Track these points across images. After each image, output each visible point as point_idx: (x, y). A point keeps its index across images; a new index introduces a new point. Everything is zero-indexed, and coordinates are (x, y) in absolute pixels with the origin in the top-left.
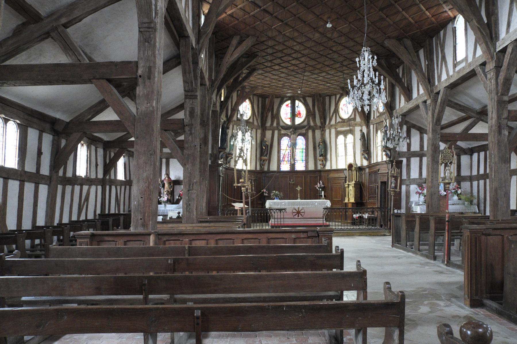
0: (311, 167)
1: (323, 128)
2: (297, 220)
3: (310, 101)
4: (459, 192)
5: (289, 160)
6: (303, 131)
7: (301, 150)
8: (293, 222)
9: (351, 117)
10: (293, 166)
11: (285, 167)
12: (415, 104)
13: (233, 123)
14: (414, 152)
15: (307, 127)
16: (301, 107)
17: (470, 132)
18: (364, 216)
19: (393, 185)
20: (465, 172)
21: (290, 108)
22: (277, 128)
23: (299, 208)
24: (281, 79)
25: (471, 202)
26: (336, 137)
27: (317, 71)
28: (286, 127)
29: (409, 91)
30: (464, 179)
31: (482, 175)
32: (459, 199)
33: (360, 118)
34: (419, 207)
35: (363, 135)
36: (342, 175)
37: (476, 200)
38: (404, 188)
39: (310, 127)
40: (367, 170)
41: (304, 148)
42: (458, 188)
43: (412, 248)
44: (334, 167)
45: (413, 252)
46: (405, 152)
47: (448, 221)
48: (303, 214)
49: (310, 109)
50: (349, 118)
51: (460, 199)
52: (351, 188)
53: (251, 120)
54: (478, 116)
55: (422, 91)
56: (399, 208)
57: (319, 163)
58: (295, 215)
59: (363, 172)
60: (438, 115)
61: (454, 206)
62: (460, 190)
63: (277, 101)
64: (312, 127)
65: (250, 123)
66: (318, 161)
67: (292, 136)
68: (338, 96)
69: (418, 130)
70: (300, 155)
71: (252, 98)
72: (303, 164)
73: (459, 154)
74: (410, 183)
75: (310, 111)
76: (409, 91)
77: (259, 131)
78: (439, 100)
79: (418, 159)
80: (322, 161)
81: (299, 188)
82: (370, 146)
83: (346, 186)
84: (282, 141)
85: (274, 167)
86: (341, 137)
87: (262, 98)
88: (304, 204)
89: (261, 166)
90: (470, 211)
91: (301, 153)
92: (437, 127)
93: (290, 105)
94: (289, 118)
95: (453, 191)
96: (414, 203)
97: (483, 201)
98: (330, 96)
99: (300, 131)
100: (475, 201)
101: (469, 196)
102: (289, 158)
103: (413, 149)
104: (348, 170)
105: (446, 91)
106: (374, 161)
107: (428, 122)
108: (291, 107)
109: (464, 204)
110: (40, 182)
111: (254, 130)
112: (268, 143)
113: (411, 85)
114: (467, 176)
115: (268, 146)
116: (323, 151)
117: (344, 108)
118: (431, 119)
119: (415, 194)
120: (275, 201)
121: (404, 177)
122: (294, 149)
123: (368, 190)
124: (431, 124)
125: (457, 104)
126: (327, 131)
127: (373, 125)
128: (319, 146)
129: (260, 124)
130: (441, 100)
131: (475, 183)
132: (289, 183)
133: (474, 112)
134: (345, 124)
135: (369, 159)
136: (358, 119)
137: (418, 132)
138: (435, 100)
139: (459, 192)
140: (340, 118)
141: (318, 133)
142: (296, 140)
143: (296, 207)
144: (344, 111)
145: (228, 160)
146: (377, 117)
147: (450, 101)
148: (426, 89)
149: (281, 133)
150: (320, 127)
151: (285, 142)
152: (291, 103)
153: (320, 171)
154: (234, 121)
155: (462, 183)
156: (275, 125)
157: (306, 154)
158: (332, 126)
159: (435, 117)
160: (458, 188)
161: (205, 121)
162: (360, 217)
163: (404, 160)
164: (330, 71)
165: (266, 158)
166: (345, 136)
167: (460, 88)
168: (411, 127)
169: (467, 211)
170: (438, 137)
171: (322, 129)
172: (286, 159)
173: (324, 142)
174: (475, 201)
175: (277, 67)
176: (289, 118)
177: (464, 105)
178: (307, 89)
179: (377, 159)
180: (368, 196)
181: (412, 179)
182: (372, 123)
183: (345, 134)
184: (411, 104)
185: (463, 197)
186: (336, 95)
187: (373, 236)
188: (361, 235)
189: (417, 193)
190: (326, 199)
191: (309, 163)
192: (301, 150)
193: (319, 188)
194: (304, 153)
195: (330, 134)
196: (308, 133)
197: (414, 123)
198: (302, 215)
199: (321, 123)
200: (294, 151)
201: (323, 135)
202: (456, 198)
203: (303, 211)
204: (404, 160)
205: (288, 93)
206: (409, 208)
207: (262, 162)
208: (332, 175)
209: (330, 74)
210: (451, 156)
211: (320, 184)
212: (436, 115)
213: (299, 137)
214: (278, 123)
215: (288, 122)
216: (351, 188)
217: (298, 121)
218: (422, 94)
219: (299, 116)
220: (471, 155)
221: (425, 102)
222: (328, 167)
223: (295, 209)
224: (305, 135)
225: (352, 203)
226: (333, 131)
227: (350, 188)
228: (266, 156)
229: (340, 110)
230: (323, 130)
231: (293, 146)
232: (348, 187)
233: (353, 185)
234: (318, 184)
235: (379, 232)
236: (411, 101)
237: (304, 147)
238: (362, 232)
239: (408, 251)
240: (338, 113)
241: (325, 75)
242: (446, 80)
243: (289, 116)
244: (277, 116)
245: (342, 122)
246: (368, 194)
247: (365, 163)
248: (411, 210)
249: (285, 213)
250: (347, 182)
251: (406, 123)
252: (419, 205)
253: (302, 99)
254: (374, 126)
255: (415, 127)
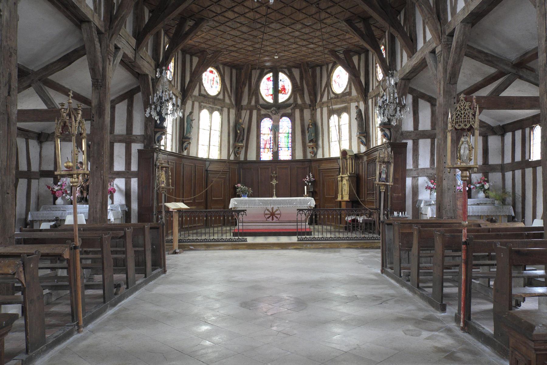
0: (299, 156)
1: (313, 106)
2: (271, 224)
3: (296, 73)
4: (487, 186)
5: (272, 147)
6: (289, 111)
7: (286, 135)
8: (261, 227)
9: (346, 91)
10: (276, 154)
11: (266, 156)
12: (420, 57)
13: (193, 98)
14: (423, 131)
15: (292, 106)
16: (285, 81)
17: (504, 94)
18: (359, 219)
19: (384, 176)
20: (494, 160)
21: (272, 82)
22: (256, 107)
23: (273, 208)
24: (246, 36)
25: (503, 202)
26: (329, 118)
27: (287, 21)
28: (267, 106)
29: (412, 40)
30: (493, 168)
31: (518, 162)
32: (486, 197)
33: (357, 90)
34: (429, 208)
35: (359, 113)
36: (335, 166)
37: (511, 198)
38: (409, 181)
39: (296, 106)
40: (365, 158)
41: (290, 132)
42: (484, 181)
43: (409, 281)
44: (327, 156)
45: (409, 289)
46: (410, 132)
47: (465, 243)
48: (278, 216)
49: (297, 83)
50: (343, 93)
51: (487, 197)
52: (345, 182)
53: (221, 97)
54: (514, 71)
55: (429, 36)
56: (403, 209)
57: (309, 150)
58: (268, 218)
59: (360, 161)
60: (453, 67)
61: (479, 207)
62: (487, 184)
63: (255, 74)
64: (299, 105)
65: (219, 100)
66: (308, 147)
67: (274, 117)
68: (330, 66)
69: (429, 101)
70: (284, 141)
71: (221, 69)
72: (289, 152)
73: (486, 134)
74: (418, 174)
75: (297, 85)
76: (412, 40)
77: (233, 112)
78: (454, 44)
79: (429, 141)
80: (313, 148)
81: (274, 182)
82: (369, 127)
83: (339, 179)
84: (262, 124)
85: (252, 157)
86: (334, 118)
87: (237, 69)
88: (280, 202)
89: (235, 155)
90: (502, 214)
91: (286, 139)
92: (452, 86)
93: (271, 79)
94: (272, 95)
95: (478, 185)
96: (423, 202)
97: (520, 199)
98: (321, 66)
99: (282, 111)
100: (509, 200)
101: (500, 192)
102: (272, 145)
103: (421, 128)
104: (342, 159)
105: (465, 28)
106: (373, 145)
107: (438, 80)
108: (273, 81)
109: (494, 204)
110: (32, 178)
111: (225, 110)
112: (245, 126)
113: (416, 32)
114: (497, 165)
115: (244, 129)
116: (313, 135)
117: (337, 80)
118: (442, 75)
119: (425, 190)
120: (242, 198)
121: (410, 165)
122: (277, 133)
123: (366, 184)
124: (442, 83)
125: (480, 52)
126: (319, 110)
127: (372, 98)
128: (308, 130)
129: (234, 102)
130: (457, 42)
131: (509, 175)
132: (271, 176)
133: (507, 65)
134: (339, 100)
135: (367, 143)
136: (354, 93)
137: (428, 104)
138: (448, 46)
139: (487, 186)
140: (333, 93)
141: (307, 113)
142: (279, 121)
143: (269, 207)
144: (337, 84)
145: (184, 146)
146: (376, 87)
147: (470, 47)
148: (434, 31)
149: (260, 113)
150: (310, 106)
151: (266, 124)
152: (273, 76)
153: (310, 161)
154: (195, 96)
155: (490, 175)
156: (253, 103)
157: (292, 140)
158: (323, 103)
159: (448, 71)
160: (484, 181)
161: (100, 81)
162: (353, 220)
163: (410, 143)
164: (306, 20)
165: (242, 144)
166: (339, 116)
167: (486, 22)
168: (418, 97)
169: (498, 214)
170: (453, 102)
171: (312, 108)
172: (268, 146)
173: (315, 125)
174: (509, 200)
175: (230, 15)
176: (272, 95)
177: (492, 54)
178: (287, 53)
179: (376, 143)
180: (366, 192)
181: (421, 169)
182: (370, 96)
183: (339, 113)
184: (415, 58)
185: (491, 194)
186: (327, 64)
187: (367, 248)
188: (350, 246)
189: (428, 188)
190: (309, 196)
191: (297, 151)
192: (286, 135)
193: (307, 182)
194: (290, 138)
195: (321, 113)
196: (294, 113)
197: (422, 91)
198: (277, 218)
199: (311, 101)
200: (277, 135)
201: (313, 116)
202: (482, 195)
203: (278, 212)
204: (410, 143)
205: (265, 61)
206: (417, 211)
207: (236, 149)
208: (324, 166)
209: (308, 26)
210: (471, 116)
211: (309, 177)
212: (449, 68)
213: (284, 118)
214: (257, 101)
215: (270, 100)
216: (345, 182)
217: (282, 98)
218: (429, 41)
219: (283, 92)
220: (503, 135)
221: (433, 52)
222: (319, 156)
223: (268, 210)
224: (291, 116)
225: (347, 201)
226: (325, 110)
227: (343, 182)
228: (242, 141)
229: (333, 83)
230: (313, 109)
231: (275, 129)
232: (342, 181)
233: (347, 178)
234: (307, 177)
235: (374, 243)
236: (415, 55)
237: (290, 131)
238: (350, 244)
239: (403, 285)
240: (331, 87)
241: (302, 28)
242: (464, 9)
243: (271, 92)
244: (255, 92)
245: (335, 98)
246: (366, 190)
247: (363, 149)
248: (420, 212)
249: (244, 215)
250: (341, 174)
251: (412, 91)
252: (430, 205)
253: (286, 71)
254: (372, 100)
255: (424, 96)
